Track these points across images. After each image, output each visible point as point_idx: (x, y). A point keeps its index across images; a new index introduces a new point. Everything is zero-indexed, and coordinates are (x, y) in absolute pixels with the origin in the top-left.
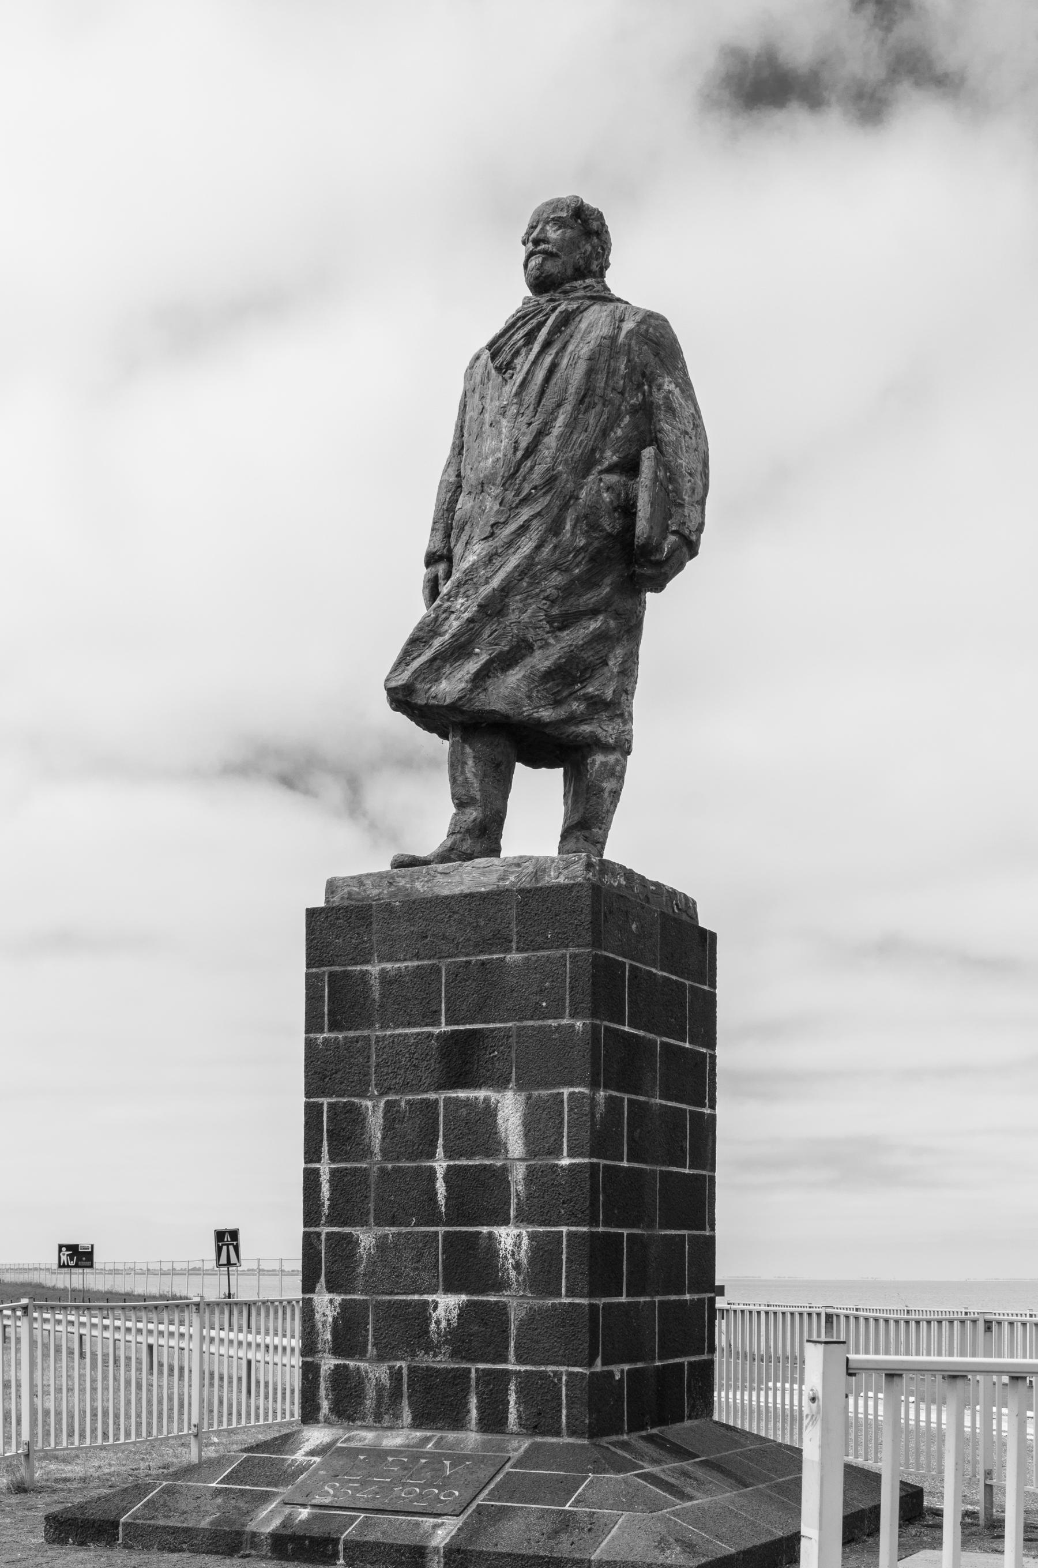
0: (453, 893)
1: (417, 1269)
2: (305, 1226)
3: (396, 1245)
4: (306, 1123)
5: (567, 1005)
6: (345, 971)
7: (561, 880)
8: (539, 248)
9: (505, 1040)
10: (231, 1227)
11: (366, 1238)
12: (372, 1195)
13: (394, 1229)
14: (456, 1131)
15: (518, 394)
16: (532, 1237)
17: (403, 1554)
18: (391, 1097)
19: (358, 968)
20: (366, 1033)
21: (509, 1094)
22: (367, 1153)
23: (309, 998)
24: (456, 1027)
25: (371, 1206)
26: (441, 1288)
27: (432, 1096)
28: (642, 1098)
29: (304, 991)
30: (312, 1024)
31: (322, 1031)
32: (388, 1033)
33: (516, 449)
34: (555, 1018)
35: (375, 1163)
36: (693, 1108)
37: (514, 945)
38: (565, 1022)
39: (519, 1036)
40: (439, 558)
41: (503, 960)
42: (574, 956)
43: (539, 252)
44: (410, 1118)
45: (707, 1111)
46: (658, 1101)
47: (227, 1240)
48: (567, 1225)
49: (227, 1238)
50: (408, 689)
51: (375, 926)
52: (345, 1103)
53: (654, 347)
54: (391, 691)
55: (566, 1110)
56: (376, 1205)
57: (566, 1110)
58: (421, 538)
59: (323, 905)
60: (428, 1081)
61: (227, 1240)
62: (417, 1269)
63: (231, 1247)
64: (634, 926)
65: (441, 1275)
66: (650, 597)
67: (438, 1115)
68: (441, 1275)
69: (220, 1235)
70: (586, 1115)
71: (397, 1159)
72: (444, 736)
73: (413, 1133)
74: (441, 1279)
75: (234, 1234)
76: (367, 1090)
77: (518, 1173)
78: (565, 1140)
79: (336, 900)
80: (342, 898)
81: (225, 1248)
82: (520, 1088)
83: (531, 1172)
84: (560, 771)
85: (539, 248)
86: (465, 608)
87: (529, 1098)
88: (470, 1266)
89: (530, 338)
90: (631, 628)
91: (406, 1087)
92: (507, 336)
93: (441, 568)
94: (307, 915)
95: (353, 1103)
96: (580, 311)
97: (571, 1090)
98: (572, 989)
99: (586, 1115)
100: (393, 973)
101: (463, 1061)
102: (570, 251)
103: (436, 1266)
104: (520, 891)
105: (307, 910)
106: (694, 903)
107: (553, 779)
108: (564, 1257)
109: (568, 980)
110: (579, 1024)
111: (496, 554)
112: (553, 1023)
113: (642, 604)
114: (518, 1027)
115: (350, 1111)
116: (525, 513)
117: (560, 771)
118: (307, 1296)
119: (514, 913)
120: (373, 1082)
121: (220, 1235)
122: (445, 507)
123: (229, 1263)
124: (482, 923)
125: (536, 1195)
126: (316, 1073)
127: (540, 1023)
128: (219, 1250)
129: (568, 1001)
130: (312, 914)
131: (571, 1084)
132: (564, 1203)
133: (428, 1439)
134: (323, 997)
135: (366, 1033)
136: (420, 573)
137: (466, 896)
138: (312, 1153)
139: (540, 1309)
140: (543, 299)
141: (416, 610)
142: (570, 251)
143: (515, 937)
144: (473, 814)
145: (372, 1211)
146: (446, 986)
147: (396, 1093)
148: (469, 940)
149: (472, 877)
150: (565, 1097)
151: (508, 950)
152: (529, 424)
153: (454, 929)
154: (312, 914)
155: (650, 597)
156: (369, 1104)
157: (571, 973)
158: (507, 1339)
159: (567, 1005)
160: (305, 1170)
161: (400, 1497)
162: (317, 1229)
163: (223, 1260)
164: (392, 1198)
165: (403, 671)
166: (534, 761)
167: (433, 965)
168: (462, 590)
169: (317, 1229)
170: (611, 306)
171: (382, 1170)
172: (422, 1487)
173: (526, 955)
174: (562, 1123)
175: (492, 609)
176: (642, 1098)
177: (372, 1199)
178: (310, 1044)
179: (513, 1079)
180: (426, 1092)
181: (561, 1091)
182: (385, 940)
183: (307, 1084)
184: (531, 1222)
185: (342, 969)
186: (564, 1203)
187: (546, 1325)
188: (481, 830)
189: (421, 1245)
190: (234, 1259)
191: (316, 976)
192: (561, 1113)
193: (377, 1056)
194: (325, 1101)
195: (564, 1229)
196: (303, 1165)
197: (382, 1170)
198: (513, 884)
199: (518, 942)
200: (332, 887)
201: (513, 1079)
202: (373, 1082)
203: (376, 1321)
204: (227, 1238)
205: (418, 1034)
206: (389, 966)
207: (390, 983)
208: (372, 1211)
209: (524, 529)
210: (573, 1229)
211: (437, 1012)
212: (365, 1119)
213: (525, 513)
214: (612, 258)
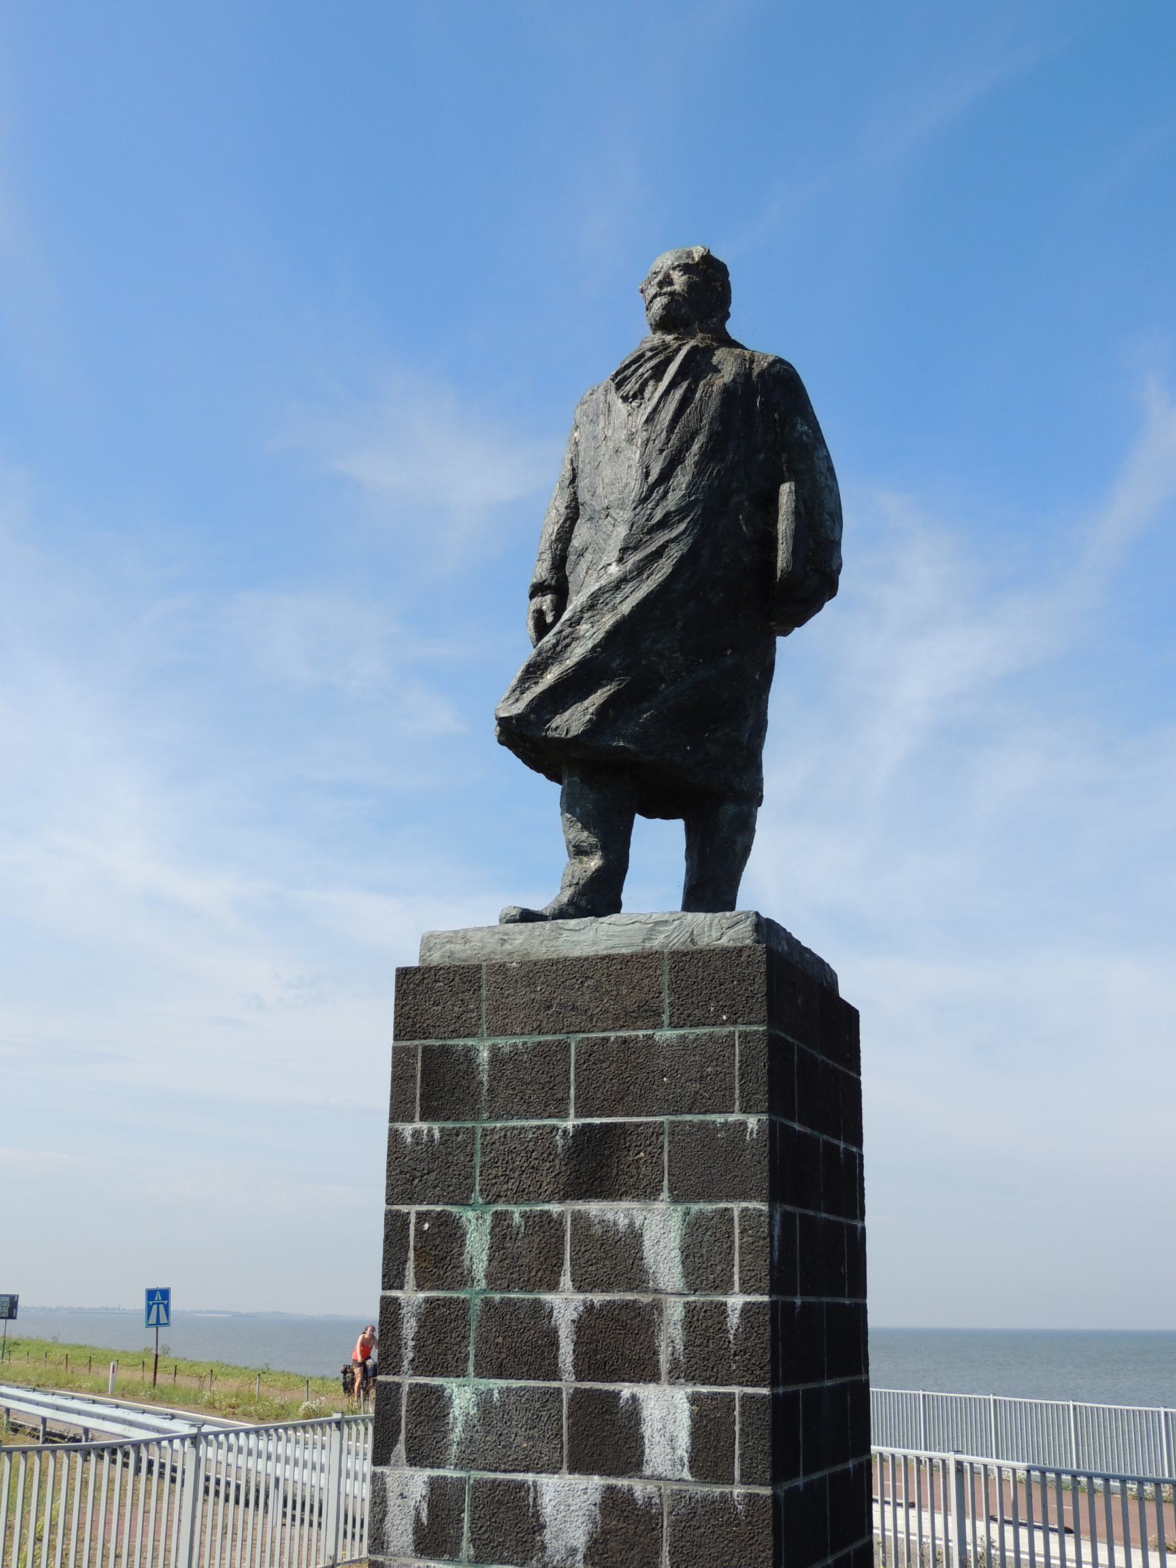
0: (585, 954)
1: (532, 1438)
3: (504, 1404)
4: (387, 1237)
5: (737, 1096)
6: (443, 1046)
7: (724, 941)
8: (665, 290)
9: (654, 1138)
11: (463, 1396)
12: (473, 1335)
13: (502, 1383)
14: (587, 1254)
15: (650, 420)
16: (694, 1399)
18: (500, 1207)
19: (460, 1042)
20: (469, 1125)
21: (662, 1205)
22: (465, 1280)
23: (396, 1078)
24: (589, 1120)
25: (471, 1349)
26: (565, 1465)
27: (555, 1208)
28: (811, 1213)
29: (390, 1069)
30: (399, 1112)
31: (411, 1120)
32: (499, 1125)
33: (647, 475)
34: (720, 1112)
35: (476, 1292)
36: (802, 1210)
37: (665, 1017)
38: (732, 1118)
39: (672, 1133)
41: (651, 1037)
42: (744, 1036)
43: (665, 294)
44: (526, 1235)
46: (824, 1215)
47: (158, 1298)
48: (740, 1384)
49: (158, 1297)
51: (484, 992)
52: (439, 1213)
55: (737, 1231)
56: (478, 1349)
57: (737, 1231)
60: (551, 1187)
61: (158, 1298)
62: (532, 1438)
63: (161, 1306)
64: (800, 1000)
65: (566, 1447)
66: (779, 640)
67: (564, 1232)
68: (566, 1447)
69: (151, 1294)
70: (764, 1238)
71: (508, 1289)
72: (554, 776)
73: (531, 1256)
74: (565, 1452)
75: (165, 1293)
76: (468, 1197)
77: (675, 1311)
78: (736, 1269)
79: (436, 958)
80: (443, 956)
81: (155, 1306)
82: (675, 1200)
83: (690, 1309)
84: (679, 824)
85: (665, 290)
86: (590, 635)
87: (687, 1213)
88: (606, 1440)
89: (658, 373)
91: (520, 1195)
92: (633, 367)
93: (546, 602)
94: (398, 976)
95: (451, 1214)
97: (744, 1205)
98: (742, 1076)
99: (764, 1238)
100: (507, 1050)
101: (597, 1166)
103: (559, 1435)
104: (674, 953)
105: (398, 970)
107: (677, 827)
108: (737, 1428)
109: (737, 1065)
110: (752, 1122)
112: (719, 1119)
114: (672, 1122)
115: (445, 1224)
116: (662, 538)
117: (679, 824)
118: (379, 1469)
119: (666, 979)
120: (477, 1188)
121: (151, 1294)
122: (553, 538)
123: (158, 1323)
124: (625, 992)
125: (698, 1342)
126: (401, 1172)
127: (701, 1117)
128: (149, 1308)
129: (737, 1091)
130: (403, 974)
131: (744, 1196)
132: (735, 1355)
134: (413, 1077)
135: (469, 1125)
137: (603, 958)
138: (392, 1277)
139: (705, 1499)
143: (667, 1010)
144: (594, 863)
145: (472, 1357)
146: (576, 1068)
147: (508, 1202)
148: (606, 1011)
149: (590, 937)
150: (736, 1213)
151: (658, 1026)
152: (661, 451)
153: (587, 997)
154: (403, 974)
155: (779, 640)
156: (471, 1214)
157: (741, 1055)
158: (658, 1540)
159: (737, 1096)
160: (383, 1298)
162: (396, 1379)
163: (153, 1320)
164: (500, 1340)
165: (517, 700)
166: (649, 814)
167: (559, 1041)
168: (586, 616)
169: (396, 1379)
171: (487, 1302)
173: (682, 1032)
174: (731, 1247)
176: (811, 1213)
177: (472, 1339)
178: (395, 1137)
179: (665, 1188)
180: (549, 1202)
181: (730, 1205)
182: (497, 1009)
183: (390, 1187)
184: (691, 1378)
185: (440, 1043)
186: (735, 1355)
187: (712, 1522)
188: (599, 895)
189: (537, 1405)
190: (163, 1320)
191: (406, 1050)
192: (730, 1235)
193: (484, 1153)
194: (413, 1209)
195: (736, 1390)
196: (379, 1292)
197: (487, 1302)
198: (664, 946)
199: (671, 1016)
200: (427, 944)
201: (665, 1188)
202: (477, 1188)
203: (474, 1508)
204: (158, 1297)
205: (538, 1128)
206: (501, 1041)
207: (503, 1062)
208: (472, 1357)
209: (658, 554)
210: (750, 1390)
211: (564, 1100)
212: (464, 1234)
214: (732, 309)
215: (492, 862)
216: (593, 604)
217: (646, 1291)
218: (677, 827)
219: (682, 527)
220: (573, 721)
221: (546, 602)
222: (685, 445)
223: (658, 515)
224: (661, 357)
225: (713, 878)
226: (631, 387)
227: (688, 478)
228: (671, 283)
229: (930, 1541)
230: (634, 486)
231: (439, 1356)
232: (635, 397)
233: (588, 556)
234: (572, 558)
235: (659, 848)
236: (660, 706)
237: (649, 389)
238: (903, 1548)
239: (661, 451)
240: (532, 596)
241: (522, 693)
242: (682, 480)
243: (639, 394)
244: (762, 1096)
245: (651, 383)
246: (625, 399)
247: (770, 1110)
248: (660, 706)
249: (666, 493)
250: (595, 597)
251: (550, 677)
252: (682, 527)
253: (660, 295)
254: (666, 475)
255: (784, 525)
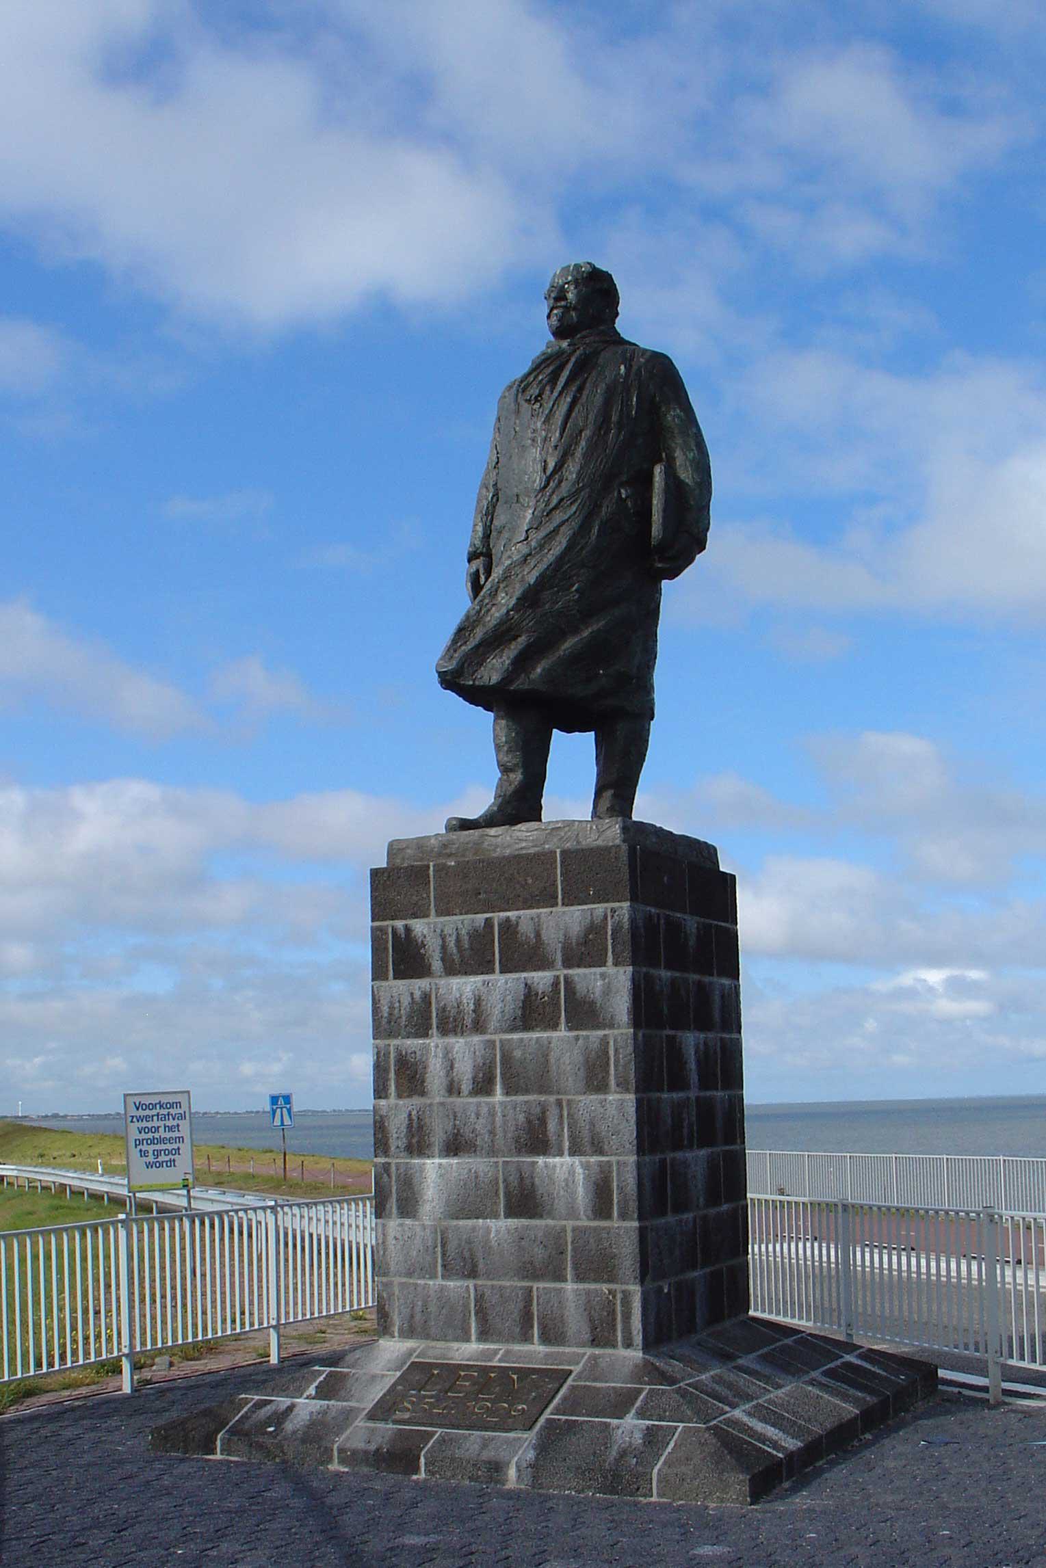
2: (373, 920)
10: (284, 1092)
17: (479, 1469)
21: (640, 1354)
40: (482, 554)
45: (734, 1036)
49: (281, 1101)
50: (459, 672)
53: (660, 381)
54: (442, 675)
58: (465, 535)
59: (385, 865)
69: (274, 1099)
75: (287, 1099)
84: (591, 735)
86: (505, 601)
90: (651, 614)
93: (479, 563)
96: (596, 353)
102: (588, 303)
106: (715, 849)
107: (587, 740)
111: (530, 555)
113: (658, 591)
116: (558, 517)
117: (591, 735)
121: (274, 1099)
130: (375, 873)
133: (496, 1352)
136: (463, 570)
138: (380, 1091)
140: (565, 344)
141: (461, 603)
142: (588, 303)
144: (517, 777)
154: (375, 873)
161: (473, 1413)
166: (568, 729)
168: (502, 586)
170: (620, 349)
172: (493, 1402)
175: (530, 599)
188: (521, 802)
191: (380, 929)
204: (281, 1101)
209: (556, 531)
211: (492, 962)
213: (558, 517)
215: (452, 767)
216: (506, 577)
217: (551, 1093)
218: (587, 740)
219: (574, 508)
220: (493, 671)
221: (479, 563)
222: (575, 440)
223: (555, 501)
224: (557, 363)
225: (618, 780)
226: (534, 391)
227: (577, 467)
228: (565, 298)
229: (1011, 1287)
230: (538, 480)
231: (418, 1145)
232: (536, 400)
233: (506, 535)
234: (494, 534)
235: (573, 758)
236: (570, 645)
237: (547, 393)
238: (817, 1271)
239: (556, 447)
240: (469, 561)
241: (455, 651)
242: (572, 470)
243: (538, 398)
244: (627, 954)
245: (548, 388)
246: (528, 401)
247: (633, 964)
248: (570, 645)
249: (560, 482)
250: (508, 569)
251: (479, 633)
252: (574, 508)
253: (557, 308)
254: (559, 467)
255: (657, 502)
